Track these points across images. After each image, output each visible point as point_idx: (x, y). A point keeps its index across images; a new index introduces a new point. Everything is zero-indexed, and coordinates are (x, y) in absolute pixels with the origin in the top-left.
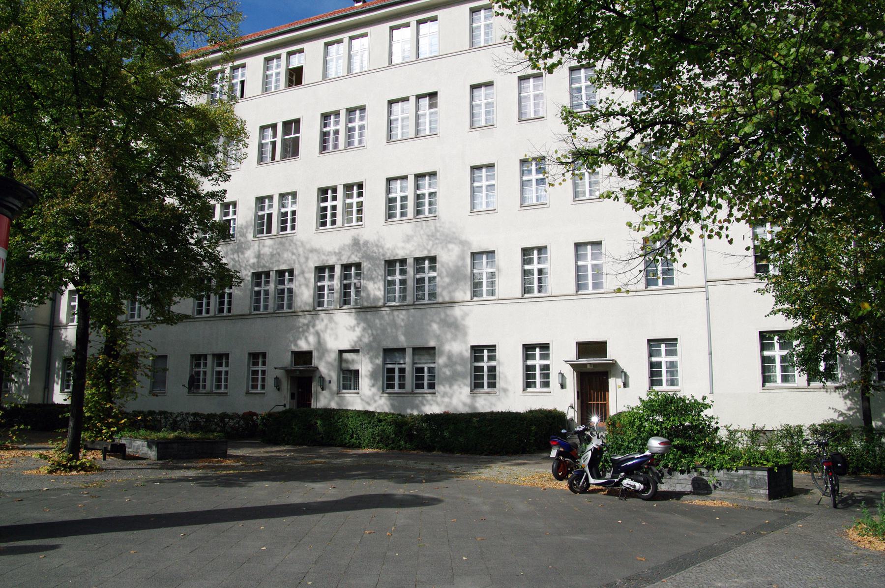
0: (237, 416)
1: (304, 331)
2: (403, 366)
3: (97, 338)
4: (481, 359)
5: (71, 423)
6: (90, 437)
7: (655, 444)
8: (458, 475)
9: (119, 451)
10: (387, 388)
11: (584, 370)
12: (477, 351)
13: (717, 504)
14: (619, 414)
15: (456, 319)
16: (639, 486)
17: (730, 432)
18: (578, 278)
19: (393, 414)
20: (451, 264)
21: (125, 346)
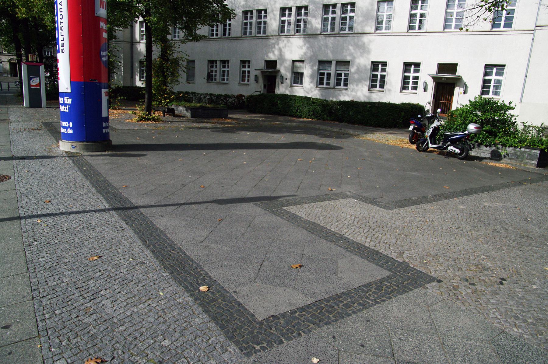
0: (234, 96)
1: (272, 48)
2: (329, 72)
3: (157, 50)
4: (377, 70)
5: (146, 96)
6: (156, 104)
7: (472, 127)
8: (354, 136)
9: (171, 112)
10: (320, 84)
11: (440, 81)
12: (375, 65)
13: (503, 166)
14: (457, 110)
15: (364, 44)
16: (457, 151)
17: (525, 126)
18: (446, 20)
19: (321, 100)
20: (364, 9)
21: (172, 54)
